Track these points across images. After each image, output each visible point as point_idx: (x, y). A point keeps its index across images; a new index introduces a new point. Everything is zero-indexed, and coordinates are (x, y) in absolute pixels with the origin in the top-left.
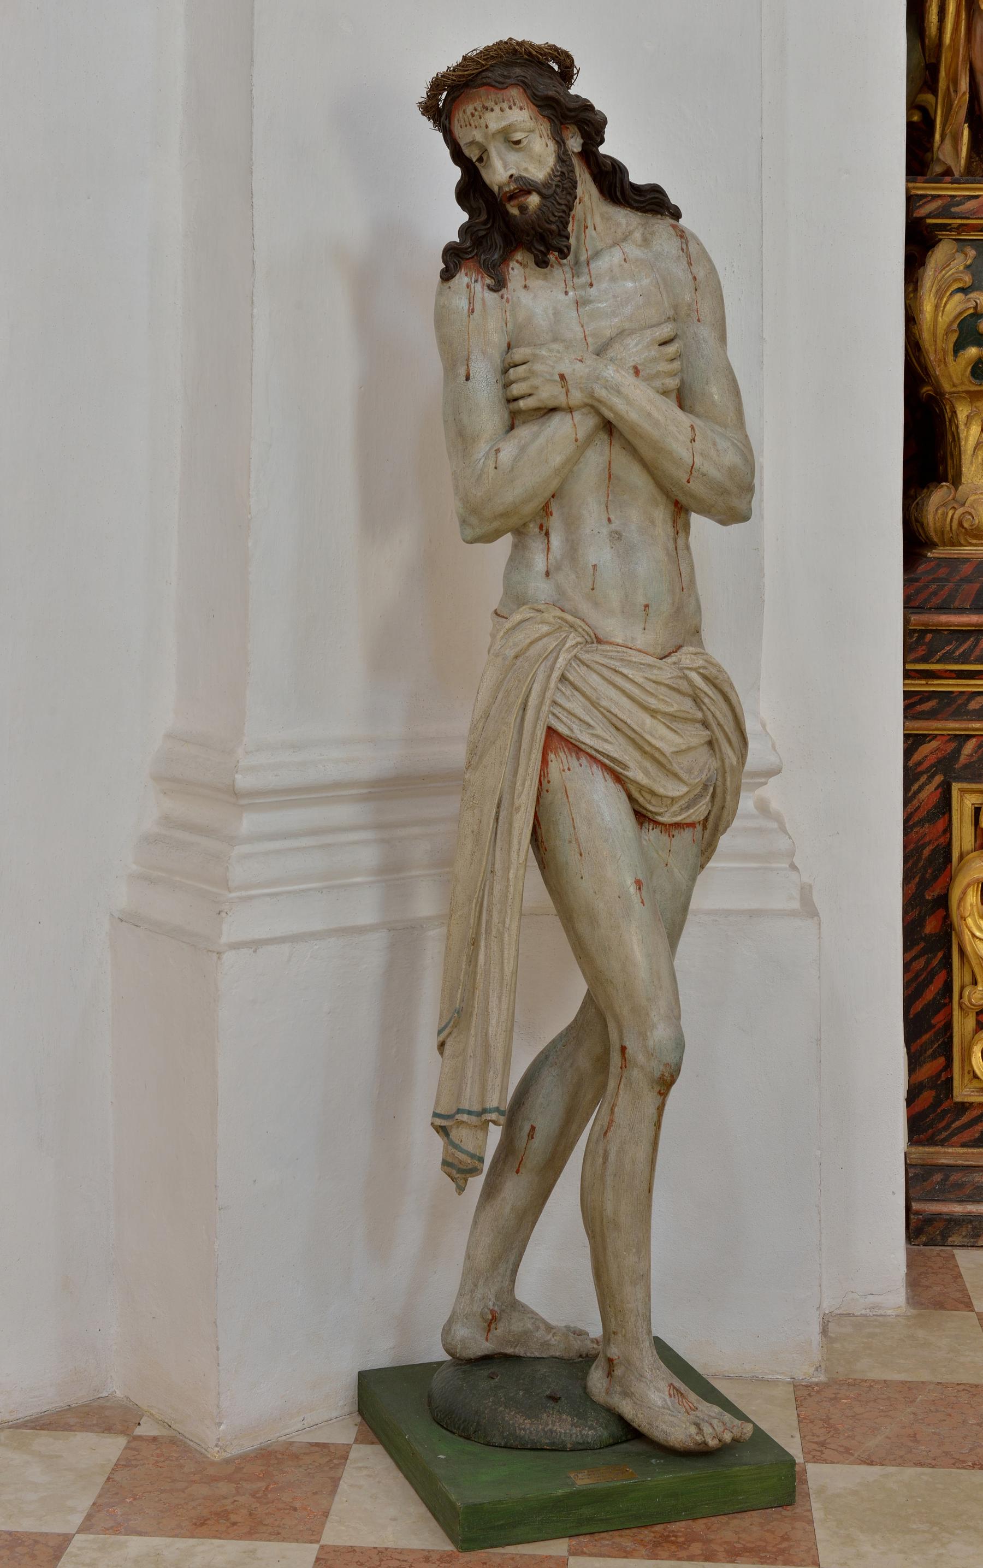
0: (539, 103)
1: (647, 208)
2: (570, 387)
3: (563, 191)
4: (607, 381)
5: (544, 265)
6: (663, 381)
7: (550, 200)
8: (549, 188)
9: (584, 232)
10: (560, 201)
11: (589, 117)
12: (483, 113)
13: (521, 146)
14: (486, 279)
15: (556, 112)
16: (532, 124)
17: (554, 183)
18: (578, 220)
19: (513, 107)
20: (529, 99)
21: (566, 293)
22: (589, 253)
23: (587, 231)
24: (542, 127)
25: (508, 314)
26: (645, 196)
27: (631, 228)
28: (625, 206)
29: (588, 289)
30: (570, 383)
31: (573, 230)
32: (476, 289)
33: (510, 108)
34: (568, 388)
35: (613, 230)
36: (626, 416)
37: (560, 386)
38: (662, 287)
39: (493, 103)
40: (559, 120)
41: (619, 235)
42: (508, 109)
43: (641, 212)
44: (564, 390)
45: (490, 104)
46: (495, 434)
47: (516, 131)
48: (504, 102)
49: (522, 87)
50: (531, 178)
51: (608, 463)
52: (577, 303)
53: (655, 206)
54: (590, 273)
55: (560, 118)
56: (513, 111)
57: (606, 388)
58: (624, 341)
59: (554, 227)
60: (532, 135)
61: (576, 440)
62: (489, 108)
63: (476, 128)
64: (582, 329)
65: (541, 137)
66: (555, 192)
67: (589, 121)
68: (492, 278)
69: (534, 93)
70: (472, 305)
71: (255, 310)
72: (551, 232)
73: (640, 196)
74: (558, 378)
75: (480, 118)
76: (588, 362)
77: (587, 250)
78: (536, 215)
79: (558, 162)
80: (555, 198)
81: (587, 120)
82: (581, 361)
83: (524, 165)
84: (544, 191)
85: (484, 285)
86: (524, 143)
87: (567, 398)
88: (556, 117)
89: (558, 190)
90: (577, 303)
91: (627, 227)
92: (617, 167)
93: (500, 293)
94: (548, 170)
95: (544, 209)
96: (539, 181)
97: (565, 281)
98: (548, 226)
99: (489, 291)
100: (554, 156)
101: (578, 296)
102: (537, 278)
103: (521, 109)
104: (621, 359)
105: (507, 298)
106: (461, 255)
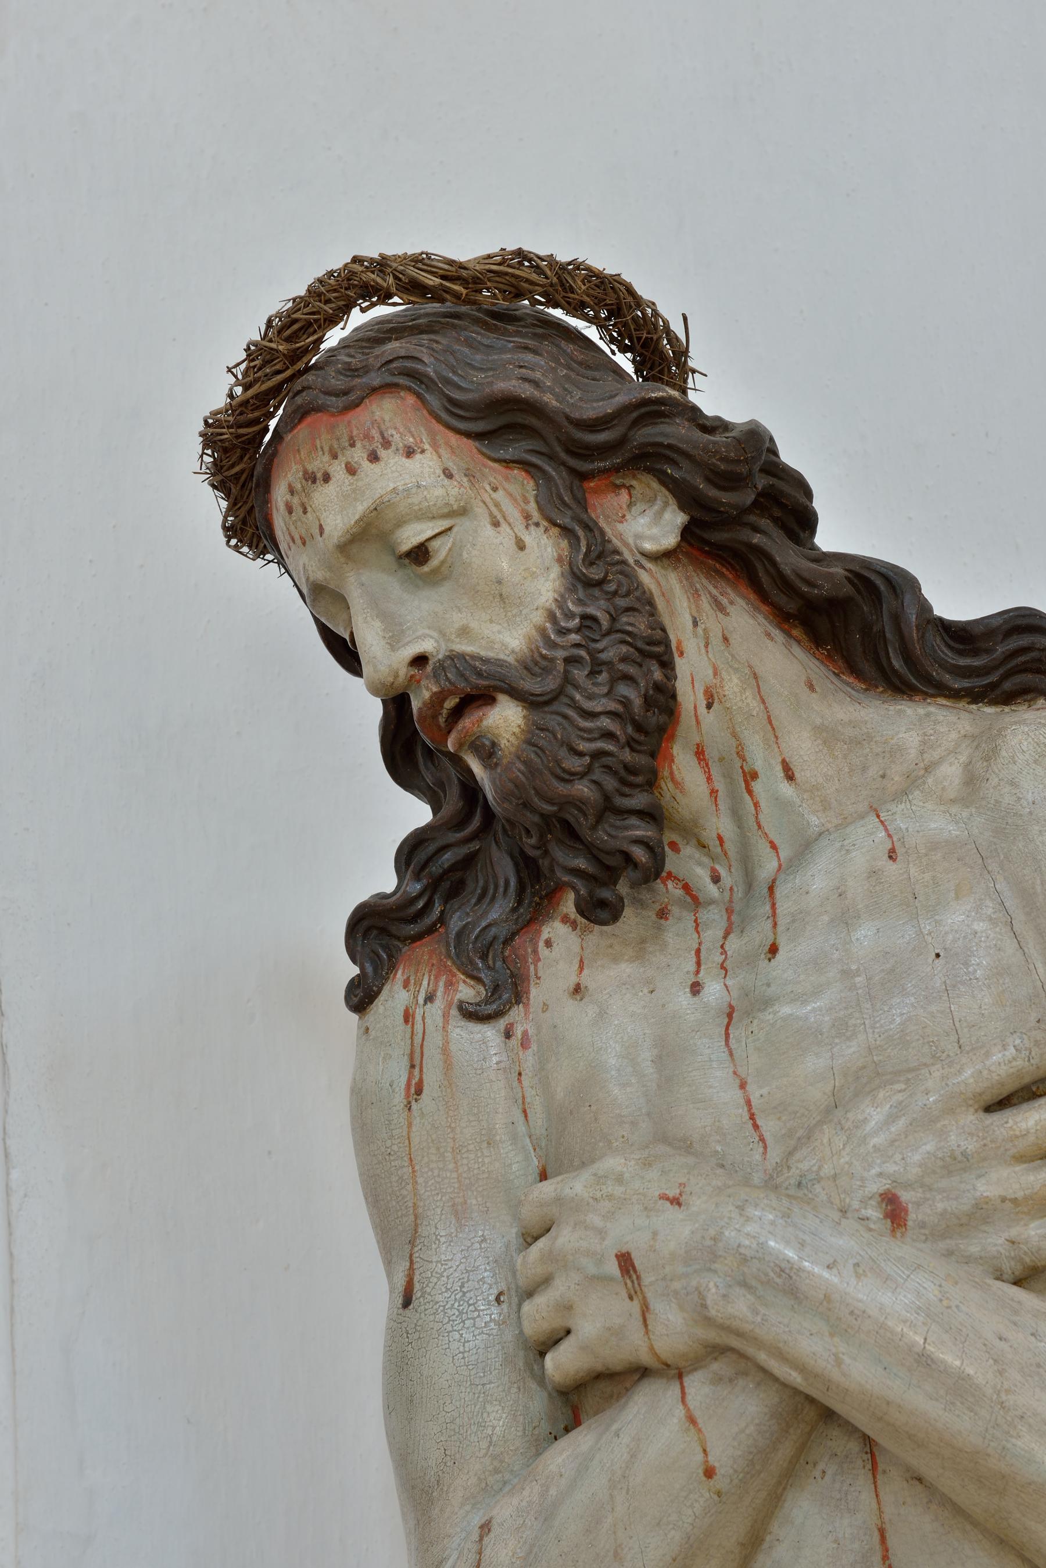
0: (480, 426)
1: (1007, 686)
2: (649, 1295)
3: (592, 673)
4: (745, 1260)
5: (604, 915)
6: (1014, 1232)
7: (555, 707)
8: (546, 671)
9: (750, 792)
10: (588, 705)
11: (666, 435)
12: (308, 495)
13: (434, 563)
14: (462, 987)
15: (545, 440)
16: (455, 492)
17: (560, 654)
18: (721, 759)
19: (382, 453)
20: (438, 419)
21: (696, 988)
22: (783, 854)
23: (757, 786)
24: (499, 495)
25: (526, 1082)
26: (988, 651)
27: (936, 754)
28: (926, 695)
29: (763, 963)
30: (647, 1279)
31: (714, 792)
32: (428, 1021)
33: (374, 458)
34: (644, 1298)
35: (873, 771)
36: (835, 1375)
37: (624, 1294)
38: (1019, 917)
39: (326, 458)
40: (564, 464)
41: (897, 777)
42: (366, 464)
43: (994, 702)
44: (635, 1306)
45: (319, 463)
46: (496, 1471)
47: (400, 523)
48: (353, 445)
49: (409, 389)
50: (483, 653)
51: (876, 1534)
52: (730, 1016)
53: (1030, 676)
54: (774, 914)
55: (563, 455)
56: (382, 463)
57: (744, 1284)
58: (850, 1115)
59: (583, 789)
60: (462, 526)
61: (709, 1473)
62: (319, 475)
63: (304, 544)
64: (739, 1093)
65: (496, 524)
66: (567, 679)
67: (670, 447)
68: (478, 980)
69: (451, 401)
70: (417, 1071)
71: (15, 1174)
72: (579, 804)
73: (975, 653)
74: (612, 1268)
75: (305, 512)
76: (697, 1204)
77: (774, 846)
78: (525, 763)
79: (572, 589)
80: (573, 699)
81: (660, 445)
82: (676, 1202)
83: (458, 619)
84: (530, 685)
85: (449, 1005)
86: (441, 550)
87: (647, 1332)
88: (551, 457)
89: (579, 674)
90: (730, 1016)
91: (922, 753)
92: (873, 577)
93: (502, 1023)
94: (538, 618)
95: (543, 739)
96: (511, 659)
97: (698, 952)
98: (562, 788)
99: (463, 1023)
100: (555, 571)
101: (735, 993)
102: (616, 959)
103: (410, 453)
104: (835, 1177)
105: (525, 1033)
106: (394, 929)
